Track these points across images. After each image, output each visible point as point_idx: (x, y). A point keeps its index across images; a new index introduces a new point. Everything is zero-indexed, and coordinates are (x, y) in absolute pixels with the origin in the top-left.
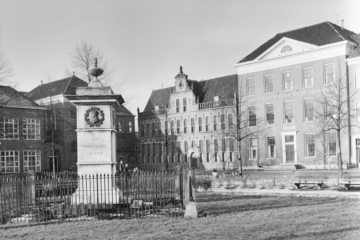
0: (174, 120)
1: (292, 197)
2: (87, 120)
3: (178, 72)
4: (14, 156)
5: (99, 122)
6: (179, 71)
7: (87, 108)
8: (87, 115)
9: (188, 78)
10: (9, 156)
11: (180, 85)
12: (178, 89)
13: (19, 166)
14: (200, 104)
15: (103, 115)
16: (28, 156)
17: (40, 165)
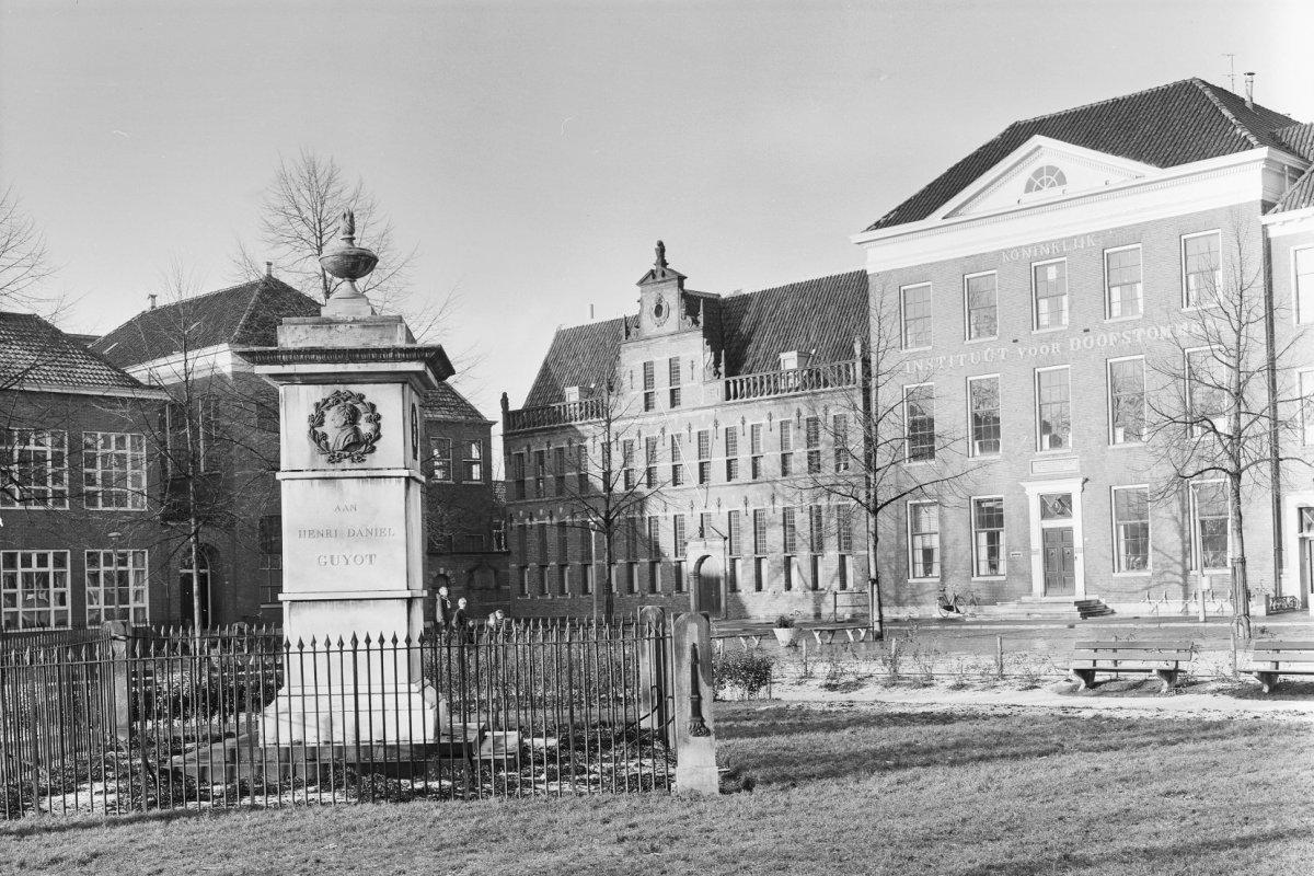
0: (634, 437)
1: (1067, 721)
2: (318, 438)
3: (650, 262)
4: (50, 568)
5: (360, 445)
6: (654, 258)
7: (318, 393)
8: (317, 420)
9: (688, 286)
10: (35, 568)
11: (658, 310)
12: (649, 324)
13: (68, 606)
14: (731, 379)
15: (376, 419)
16: (103, 569)
17: (146, 604)
